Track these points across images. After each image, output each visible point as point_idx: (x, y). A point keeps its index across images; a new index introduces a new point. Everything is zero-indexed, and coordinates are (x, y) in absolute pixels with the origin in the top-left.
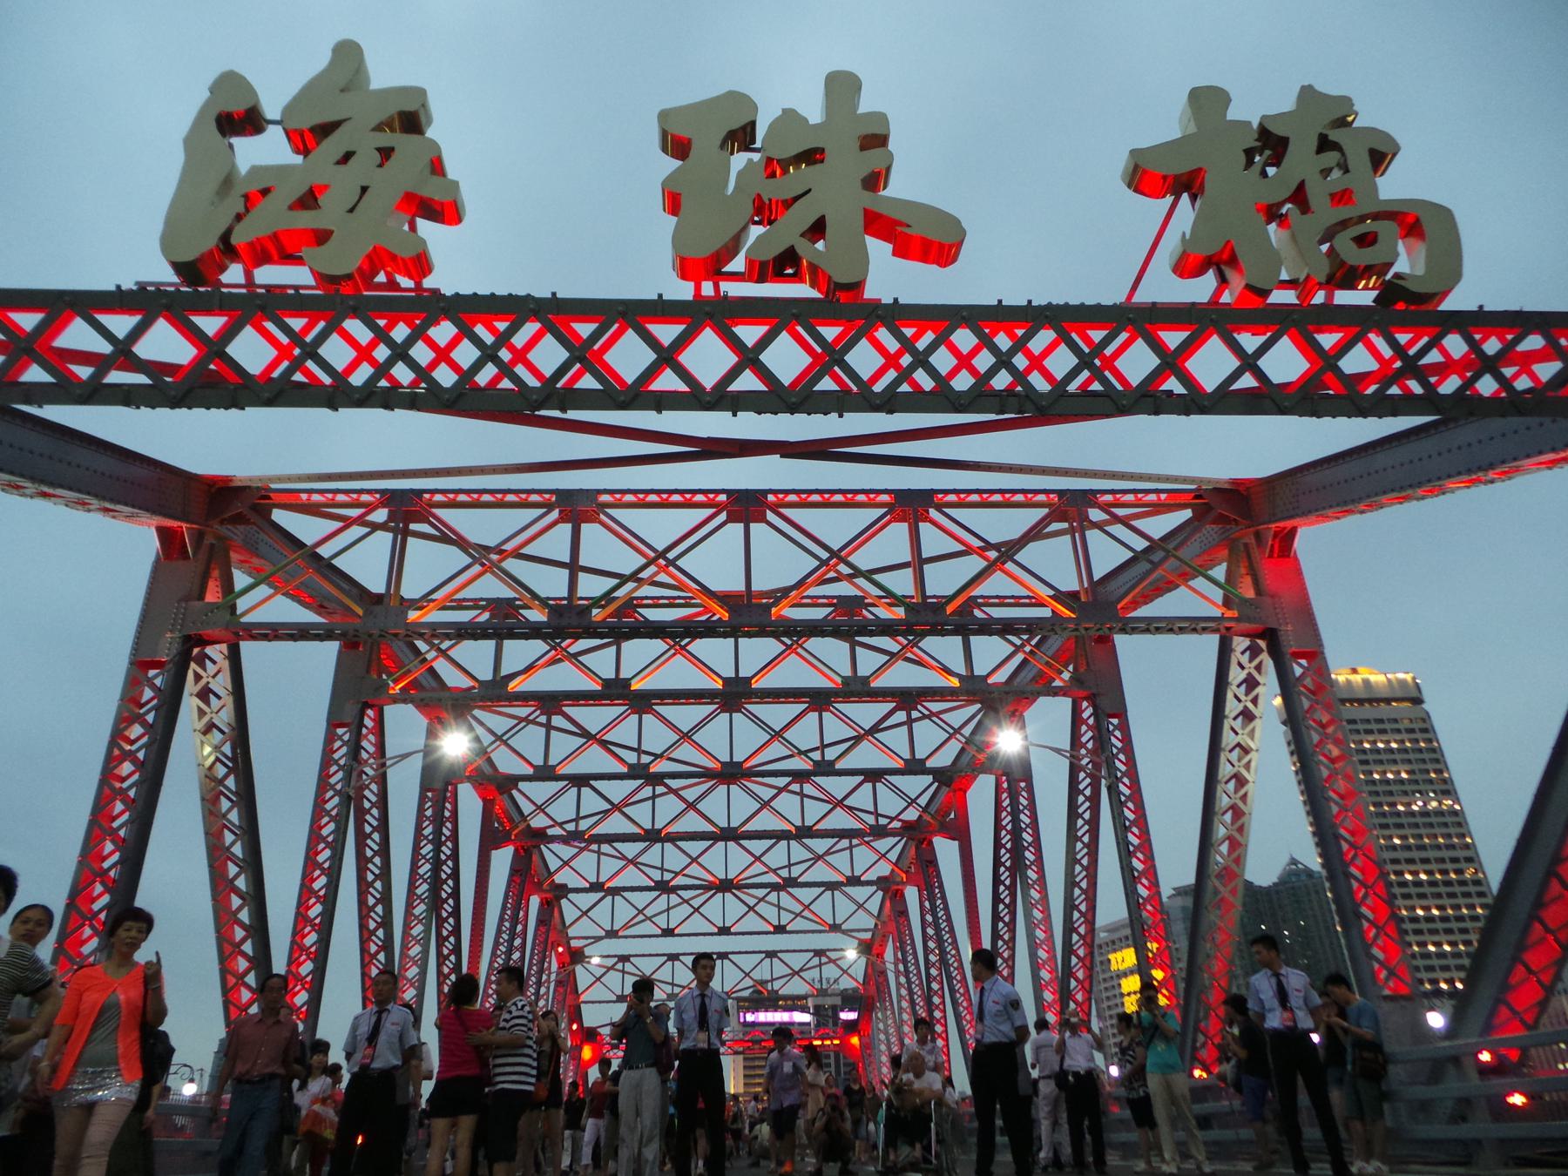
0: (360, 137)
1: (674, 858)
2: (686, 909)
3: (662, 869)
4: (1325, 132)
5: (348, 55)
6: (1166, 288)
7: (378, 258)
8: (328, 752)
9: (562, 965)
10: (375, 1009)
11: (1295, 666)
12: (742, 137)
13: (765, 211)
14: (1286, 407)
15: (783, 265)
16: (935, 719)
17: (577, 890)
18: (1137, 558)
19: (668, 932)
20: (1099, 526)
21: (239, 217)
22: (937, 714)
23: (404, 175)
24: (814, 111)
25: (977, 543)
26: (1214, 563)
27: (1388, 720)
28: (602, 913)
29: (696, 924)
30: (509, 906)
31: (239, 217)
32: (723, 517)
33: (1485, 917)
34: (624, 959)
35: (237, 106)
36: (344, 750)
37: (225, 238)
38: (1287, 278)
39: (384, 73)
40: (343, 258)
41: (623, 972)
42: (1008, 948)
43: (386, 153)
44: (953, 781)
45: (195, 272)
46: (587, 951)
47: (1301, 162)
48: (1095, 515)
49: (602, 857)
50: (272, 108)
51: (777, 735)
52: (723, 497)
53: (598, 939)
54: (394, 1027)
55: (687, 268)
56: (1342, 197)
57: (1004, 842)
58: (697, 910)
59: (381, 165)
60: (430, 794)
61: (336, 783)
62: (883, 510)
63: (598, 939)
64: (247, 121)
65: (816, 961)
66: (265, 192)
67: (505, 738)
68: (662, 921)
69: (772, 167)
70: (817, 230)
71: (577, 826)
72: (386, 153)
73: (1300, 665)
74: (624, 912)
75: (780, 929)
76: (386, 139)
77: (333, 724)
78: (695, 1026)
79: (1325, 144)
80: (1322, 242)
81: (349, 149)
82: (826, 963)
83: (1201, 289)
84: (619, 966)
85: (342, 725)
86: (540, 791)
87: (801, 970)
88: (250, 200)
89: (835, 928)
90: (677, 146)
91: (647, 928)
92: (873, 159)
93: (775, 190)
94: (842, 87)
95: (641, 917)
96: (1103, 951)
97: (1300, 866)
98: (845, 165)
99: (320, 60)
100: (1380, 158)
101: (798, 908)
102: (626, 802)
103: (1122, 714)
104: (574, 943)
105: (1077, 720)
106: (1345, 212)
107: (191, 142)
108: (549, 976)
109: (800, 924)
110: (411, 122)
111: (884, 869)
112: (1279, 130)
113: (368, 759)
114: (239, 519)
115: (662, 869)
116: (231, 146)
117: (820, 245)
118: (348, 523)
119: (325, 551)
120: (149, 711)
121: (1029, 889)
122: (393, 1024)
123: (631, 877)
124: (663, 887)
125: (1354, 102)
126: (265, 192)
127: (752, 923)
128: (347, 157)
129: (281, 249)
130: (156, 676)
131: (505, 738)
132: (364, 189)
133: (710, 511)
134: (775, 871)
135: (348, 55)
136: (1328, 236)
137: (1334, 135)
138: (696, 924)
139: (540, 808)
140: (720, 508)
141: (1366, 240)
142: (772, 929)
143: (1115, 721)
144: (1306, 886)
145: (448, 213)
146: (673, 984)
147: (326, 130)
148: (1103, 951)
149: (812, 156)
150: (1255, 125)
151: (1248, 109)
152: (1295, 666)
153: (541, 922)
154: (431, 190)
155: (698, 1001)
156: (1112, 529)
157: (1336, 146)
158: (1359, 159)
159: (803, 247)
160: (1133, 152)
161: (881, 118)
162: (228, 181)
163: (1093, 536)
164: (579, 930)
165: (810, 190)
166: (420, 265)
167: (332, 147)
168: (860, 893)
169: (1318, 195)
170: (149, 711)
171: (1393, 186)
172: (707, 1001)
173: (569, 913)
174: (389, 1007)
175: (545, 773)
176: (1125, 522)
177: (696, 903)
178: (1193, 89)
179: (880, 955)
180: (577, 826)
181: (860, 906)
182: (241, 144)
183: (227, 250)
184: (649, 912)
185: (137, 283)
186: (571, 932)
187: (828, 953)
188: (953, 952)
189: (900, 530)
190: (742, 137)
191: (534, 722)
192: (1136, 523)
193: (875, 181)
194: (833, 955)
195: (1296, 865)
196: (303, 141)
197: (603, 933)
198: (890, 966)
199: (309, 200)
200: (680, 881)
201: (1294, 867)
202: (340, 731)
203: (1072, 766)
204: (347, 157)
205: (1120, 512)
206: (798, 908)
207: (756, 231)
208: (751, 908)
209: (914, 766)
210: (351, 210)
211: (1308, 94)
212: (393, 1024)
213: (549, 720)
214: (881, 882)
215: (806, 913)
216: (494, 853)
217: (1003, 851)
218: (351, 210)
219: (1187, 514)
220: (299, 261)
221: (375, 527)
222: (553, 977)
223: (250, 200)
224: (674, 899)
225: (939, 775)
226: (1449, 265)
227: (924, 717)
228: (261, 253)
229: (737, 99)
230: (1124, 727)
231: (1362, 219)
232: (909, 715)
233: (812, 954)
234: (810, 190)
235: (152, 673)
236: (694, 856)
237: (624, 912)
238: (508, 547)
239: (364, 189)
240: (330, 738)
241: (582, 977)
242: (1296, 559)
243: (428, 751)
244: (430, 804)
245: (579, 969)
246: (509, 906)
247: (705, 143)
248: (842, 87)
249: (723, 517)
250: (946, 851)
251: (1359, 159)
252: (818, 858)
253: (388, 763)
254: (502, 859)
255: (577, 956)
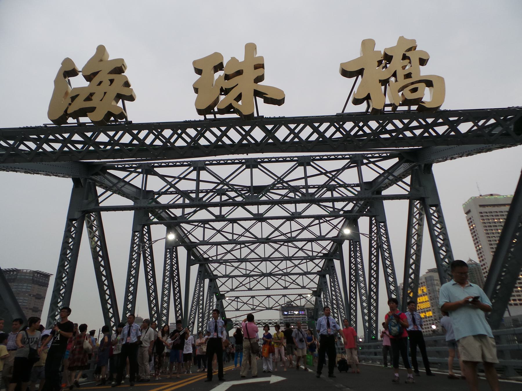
0: (104, 76)
1: (250, 267)
2: (255, 282)
3: (246, 270)
4: (405, 53)
5: (101, 49)
6: (352, 109)
7: (109, 114)
8: (133, 240)
9: (218, 299)
10: (129, 326)
11: (430, 210)
12: (219, 67)
13: (225, 91)
14: (387, 146)
15: (229, 109)
16: (328, 222)
17: (220, 277)
18: (381, 175)
19: (250, 289)
20: (366, 164)
21: (70, 104)
22: (329, 221)
23: (118, 88)
24: (241, 58)
25: (324, 171)
26: (405, 176)
27: (499, 211)
28: (229, 283)
29: (259, 287)
30: (198, 282)
31: (70, 104)
32: (244, 167)
33: (516, 284)
34: (237, 297)
35: (70, 69)
36: (138, 239)
37: (66, 111)
38: (389, 103)
39: (112, 55)
40: (99, 115)
41: (237, 301)
42: (355, 295)
43: (112, 81)
44: (338, 241)
45: (60, 121)
46: (226, 295)
47: (397, 64)
48: (365, 161)
49: (227, 266)
50: (79, 67)
51: (277, 229)
52: (244, 161)
53: (228, 292)
54: (134, 331)
55: (200, 112)
56: (408, 76)
57: (373, 252)
58: (259, 282)
59: (110, 85)
60: (168, 250)
61: (136, 250)
62: (296, 162)
63: (228, 292)
64: (74, 73)
65: (299, 298)
66: (77, 95)
67: (190, 232)
68: (248, 286)
69: (227, 77)
70: (239, 98)
71: (241, 246)
72: (112, 81)
73: (432, 210)
74: (236, 283)
75: (286, 288)
76: (112, 76)
77: (134, 232)
78: (214, 331)
79: (405, 57)
80: (399, 91)
81: (92, 92)
82: (302, 298)
83: (362, 108)
84: (236, 300)
85: (137, 232)
86: (204, 248)
87: (294, 300)
88: (73, 98)
89: (303, 287)
90: (199, 71)
91: (243, 288)
92: (259, 72)
93: (227, 84)
94: (251, 48)
95: (241, 285)
96: (423, 285)
97: (473, 262)
98: (250, 74)
99: (93, 52)
100: (423, 62)
101: (292, 281)
102: (232, 250)
103: (385, 222)
104: (221, 293)
105: (371, 224)
106: (409, 81)
107: (56, 82)
108: (213, 303)
109: (293, 286)
110: (119, 69)
111: (318, 269)
112: (389, 54)
113: (146, 241)
114: (97, 174)
115: (246, 270)
116: (69, 80)
117: (240, 103)
118: (131, 172)
119: (127, 180)
120: (73, 234)
121: (359, 277)
122: (134, 330)
123: (236, 273)
124: (247, 276)
125: (416, 41)
126: (77, 95)
127: (277, 286)
128: (100, 83)
129: (83, 112)
130: (75, 223)
131: (190, 232)
132: (105, 93)
133: (240, 165)
134: (282, 270)
135: (101, 49)
136: (402, 89)
137: (408, 54)
138: (259, 287)
139: (205, 253)
140: (243, 164)
141: (415, 90)
142: (255, 297)
143: (382, 224)
144: (475, 268)
145: (131, 98)
146: (253, 305)
147: (95, 74)
148: (423, 285)
149: (239, 73)
150: (383, 53)
151: (381, 47)
152: (430, 210)
153: (210, 287)
154: (124, 91)
155: (215, 324)
156: (370, 165)
157: (409, 58)
158: (415, 61)
159: (234, 104)
160: (341, 64)
161: (262, 58)
162: (67, 93)
163: (364, 168)
164: (222, 289)
165: (238, 84)
166: (122, 115)
167: (96, 80)
168: (312, 277)
169: (401, 74)
170: (73, 234)
171: (425, 71)
172: (217, 323)
173: (219, 284)
174: (133, 325)
175: (204, 243)
176: (373, 163)
177: (259, 280)
178: (364, 40)
179: (320, 296)
180: (241, 246)
181: (312, 280)
182: (71, 79)
183: (66, 115)
184: (243, 283)
185: (44, 124)
186: (220, 289)
187: (303, 295)
188: (340, 296)
189: (301, 168)
190: (219, 67)
191: (200, 226)
192: (377, 163)
193: (261, 78)
194: (304, 296)
195: (471, 261)
196: (89, 78)
197: (229, 290)
198: (323, 300)
199: (89, 98)
200: (253, 273)
201: (471, 262)
202: (136, 234)
203: (370, 239)
204: (100, 83)
205: (372, 160)
206: (292, 281)
207: (222, 97)
208: (276, 282)
209: (322, 238)
210: (101, 100)
211: (401, 39)
212: (134, 330)
213: (204, 226)
214: (318, 273)
215: (294, 283)
216: (191, 267)
217: (373, 256)
218: (101, 100)
219: (396, 160)
220: (86, 116)
221: (139, 173)
222: (215, 303)
223: (73, 98)
224: (252, 279)
225: (332, 239)
226: (441, 95)
227: (324, 222)
228: (76, 115)
229: (217, 55)
230: (385, 226)
231: (413, 83)
232: (319, 221)
233: (298, 295)
234: (238, 84)
235: (74, 222)
236: (256, 266)
237: (236, 283)
238: (182, 176)
239: (105, 93)
240: (134, 236)
241: (225, 304)
242: (433, 174)
243: (166, 238)
244: (168, 253)
245: (223, 301)
246: (198, 282)
247: (208, 69)
248: (251, 48)
249: (244, 167)
250: (337, 263)
251: (415, 61)
252: (296, 266)
253: (152, 243)
254: (195, 269)
255: (223, 297)
